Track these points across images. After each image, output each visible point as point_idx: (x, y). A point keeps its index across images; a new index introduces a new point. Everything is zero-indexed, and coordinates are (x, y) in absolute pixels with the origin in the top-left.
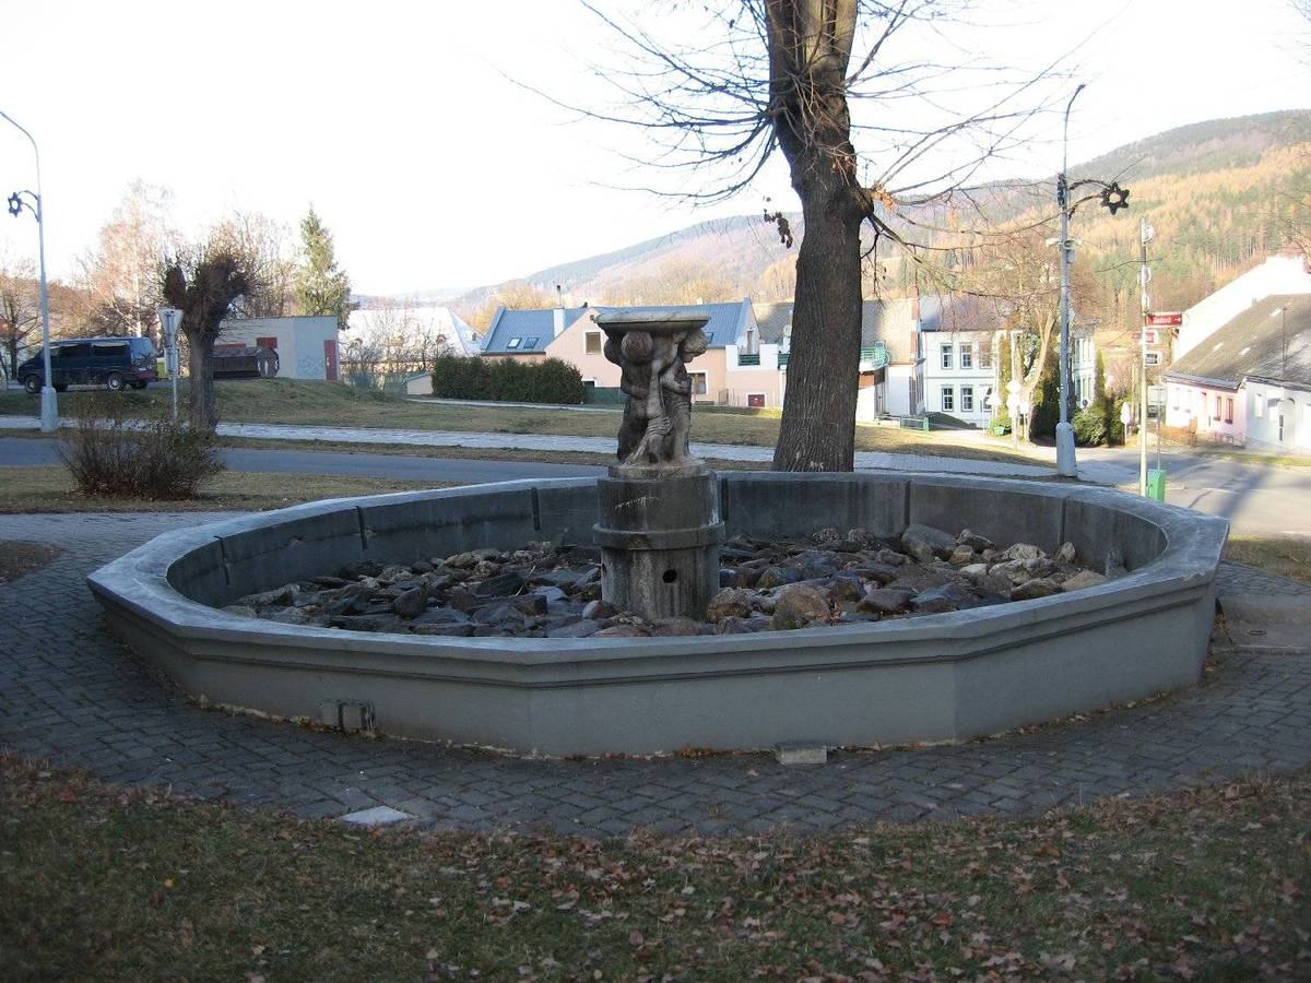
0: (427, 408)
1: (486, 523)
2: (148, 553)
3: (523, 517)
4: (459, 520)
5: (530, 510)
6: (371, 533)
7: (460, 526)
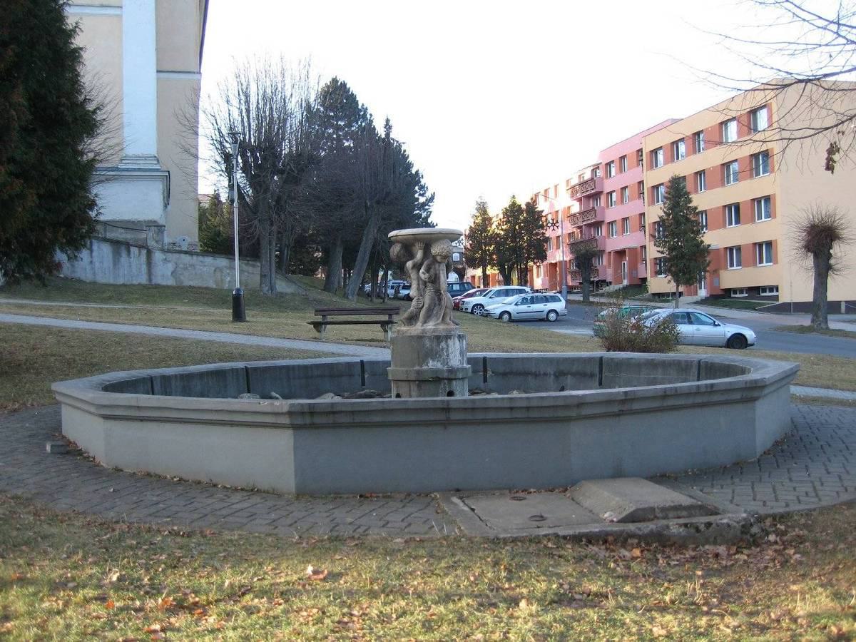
0: (167, 321)
1: (569, 376)
2: (73, 253)
3: (592, 375)
4: (552, 373)
5: (597, 370)
6: (491, 373)
7: (552, 377)
